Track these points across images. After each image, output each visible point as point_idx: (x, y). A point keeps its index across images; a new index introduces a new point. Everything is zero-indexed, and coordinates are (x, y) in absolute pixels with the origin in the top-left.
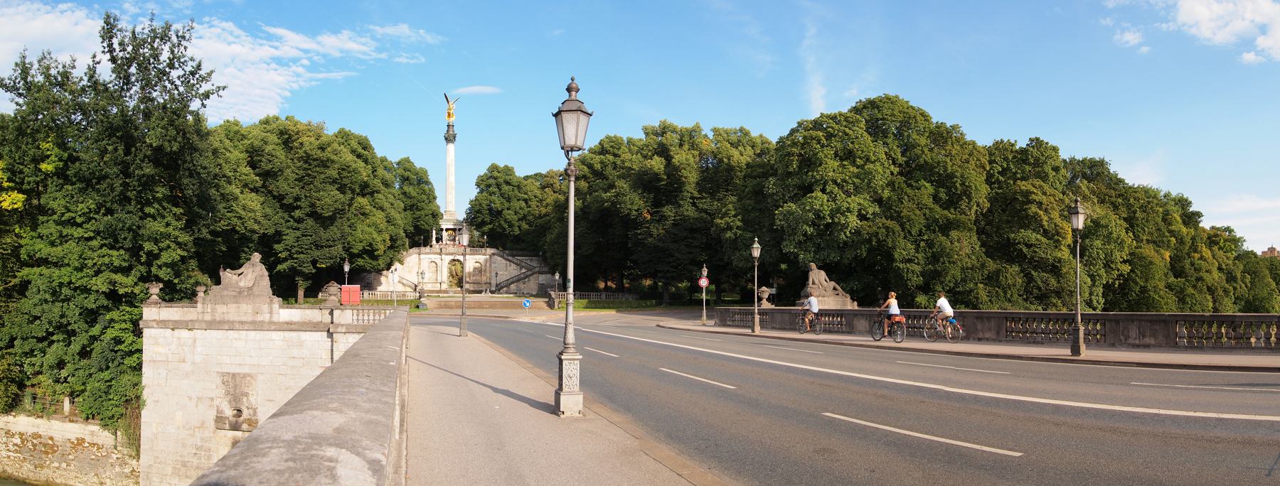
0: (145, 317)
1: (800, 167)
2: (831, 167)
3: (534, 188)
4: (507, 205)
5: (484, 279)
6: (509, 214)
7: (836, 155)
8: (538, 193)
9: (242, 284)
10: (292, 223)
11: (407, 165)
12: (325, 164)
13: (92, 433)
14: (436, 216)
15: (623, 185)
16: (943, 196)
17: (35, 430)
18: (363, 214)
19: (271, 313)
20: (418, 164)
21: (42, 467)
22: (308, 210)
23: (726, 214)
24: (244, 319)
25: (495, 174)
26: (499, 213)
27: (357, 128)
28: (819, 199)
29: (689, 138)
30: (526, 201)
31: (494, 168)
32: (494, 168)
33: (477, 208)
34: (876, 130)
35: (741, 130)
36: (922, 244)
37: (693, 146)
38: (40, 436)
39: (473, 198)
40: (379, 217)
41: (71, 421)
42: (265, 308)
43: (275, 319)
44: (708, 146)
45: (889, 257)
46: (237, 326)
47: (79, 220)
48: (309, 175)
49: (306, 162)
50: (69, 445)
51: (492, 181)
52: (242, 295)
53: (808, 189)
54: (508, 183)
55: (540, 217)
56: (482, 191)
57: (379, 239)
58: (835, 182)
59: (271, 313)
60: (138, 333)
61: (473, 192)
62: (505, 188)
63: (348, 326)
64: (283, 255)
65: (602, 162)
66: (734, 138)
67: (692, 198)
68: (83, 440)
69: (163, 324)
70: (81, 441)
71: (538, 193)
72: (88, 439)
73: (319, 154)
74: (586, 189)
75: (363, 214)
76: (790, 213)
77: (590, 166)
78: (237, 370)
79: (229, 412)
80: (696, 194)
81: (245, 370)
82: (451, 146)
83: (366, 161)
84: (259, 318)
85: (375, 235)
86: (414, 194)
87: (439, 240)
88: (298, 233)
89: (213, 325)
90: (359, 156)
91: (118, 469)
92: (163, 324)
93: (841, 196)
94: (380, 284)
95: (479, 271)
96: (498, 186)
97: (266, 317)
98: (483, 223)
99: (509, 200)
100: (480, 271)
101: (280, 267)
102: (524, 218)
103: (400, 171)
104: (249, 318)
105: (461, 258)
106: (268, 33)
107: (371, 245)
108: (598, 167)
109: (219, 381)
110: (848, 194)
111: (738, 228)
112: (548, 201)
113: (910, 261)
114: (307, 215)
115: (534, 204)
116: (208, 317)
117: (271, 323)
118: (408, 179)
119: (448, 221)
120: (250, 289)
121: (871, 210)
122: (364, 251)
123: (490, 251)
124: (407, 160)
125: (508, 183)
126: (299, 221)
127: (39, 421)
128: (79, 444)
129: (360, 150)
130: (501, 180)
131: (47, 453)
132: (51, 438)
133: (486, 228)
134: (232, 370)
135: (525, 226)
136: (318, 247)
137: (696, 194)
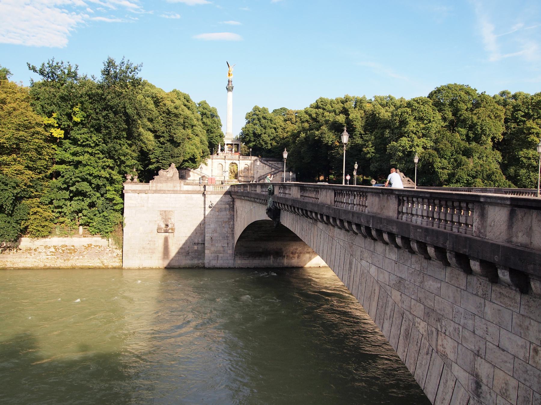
0: (125, 188)
1: (400, 125)
2: (412, 125)
3: (279, 120)
4: (264, 131)
5: (250, 175)
6: (265, 137)
7: (415, 119)
8: (282, 124)
9: (168, 176)
10: (159, 144)
11: (205, 106)
12: (176, 116)
13: (96, 241)
14: (221, 136)
15: (324, 128)
16: (471, 135)
17: (63, 243)
18: (189, 138)
19: (180, 187)
20: (212, 104)
21: (68, 260)
22: (168, 138)
23: (367, 146)
24: (169, 189)
25: (257, 112)
26: (260, 136)
27: (183, 90)
28: (404, 141)
29: (359, 103)
30: (275, 129)
31: (256, 109)
32: (256, 109)
33: (247, 132)
34: (439, 106)
35: (389, 97)
36: (452, 160)
37: (361, 108)
38: (66, 246)
39: (244, 126)
40: (197, 140)
41: (84, 237)
42: (178, 185)
43: (182, 189)
44: (368, 107)
45: (432, 164)
46: (167, 192)
47: (93, 145)
48: (168, 121)
49: (168, 114)
50: (83, 248)
51: (255, 117)
52: (167, 180)
53: (402, 135)
54: (265, 118)
55: (283, 139)
56: (249, 122)
57: (198, 152)
58: (412, 132)
59: (180, 187)
60: (122, 196)
61: (243, 123)
62: (263, 121)
63: (211, 192)
64: (154, 160)
65: (316, 113)
66: (384, 102)
67: (361, 134)
68: (91, 245)
69: (134, 191)
70: (90, 246)
71: (282, 124)
72: (94, 244)
73: (175, 111)
74: (308, 127)
75: (189, 138)
76: (394, 146)
77: (310, 115)
78: (166, 209)
79: (163, 226)
80: (363, 132)
81: (170, 209)
82: (230, 93)
83: (189, 108)
84: (176, 189)
85: (196, 151)
86: (209, 123)
87: (222, 150)
88: (162, 150)
89: (156, 192)
90: (185, 105)
91: (110, 255)
92: (134, 191)
93: (416, 139)
94: (189, 176)
95: (247, 169)
96: (259, 119)
97: (178, 189)
98: (250, 141)
99: (265, 128)
100: (248, 170)
101: (150, 167)
102: (274, 139)
103: (201, 109)
104: (172, 189)
105: (237, 162)
106: (370, 221)
107: (193, 156)
108: (314, 116)
109: (159, 214)
110: (419, 138)
111: (372, 152)
112: (288, 129)
113: (443, 168)
114: (167, 141)
115: (280, 130)
116: (154, 189)
117: (180, 191)
118: (205, 114)
119: (228, 139)
120: (172, 177)
121: (429, 145)
122: (190, 159)
123: (254, 158)
124: (205, 102)
125: (265, 118)
126: (163, 143)
127: (66, 239)
128: (89, 247)
129: (186, 103)
130: (261, 116)
131: (71, 253)
132: (73, 246)
133: (251, 145)
134: (164, 209)
135: (274, 144)
136: (172, 157)
137: (363, 132)
